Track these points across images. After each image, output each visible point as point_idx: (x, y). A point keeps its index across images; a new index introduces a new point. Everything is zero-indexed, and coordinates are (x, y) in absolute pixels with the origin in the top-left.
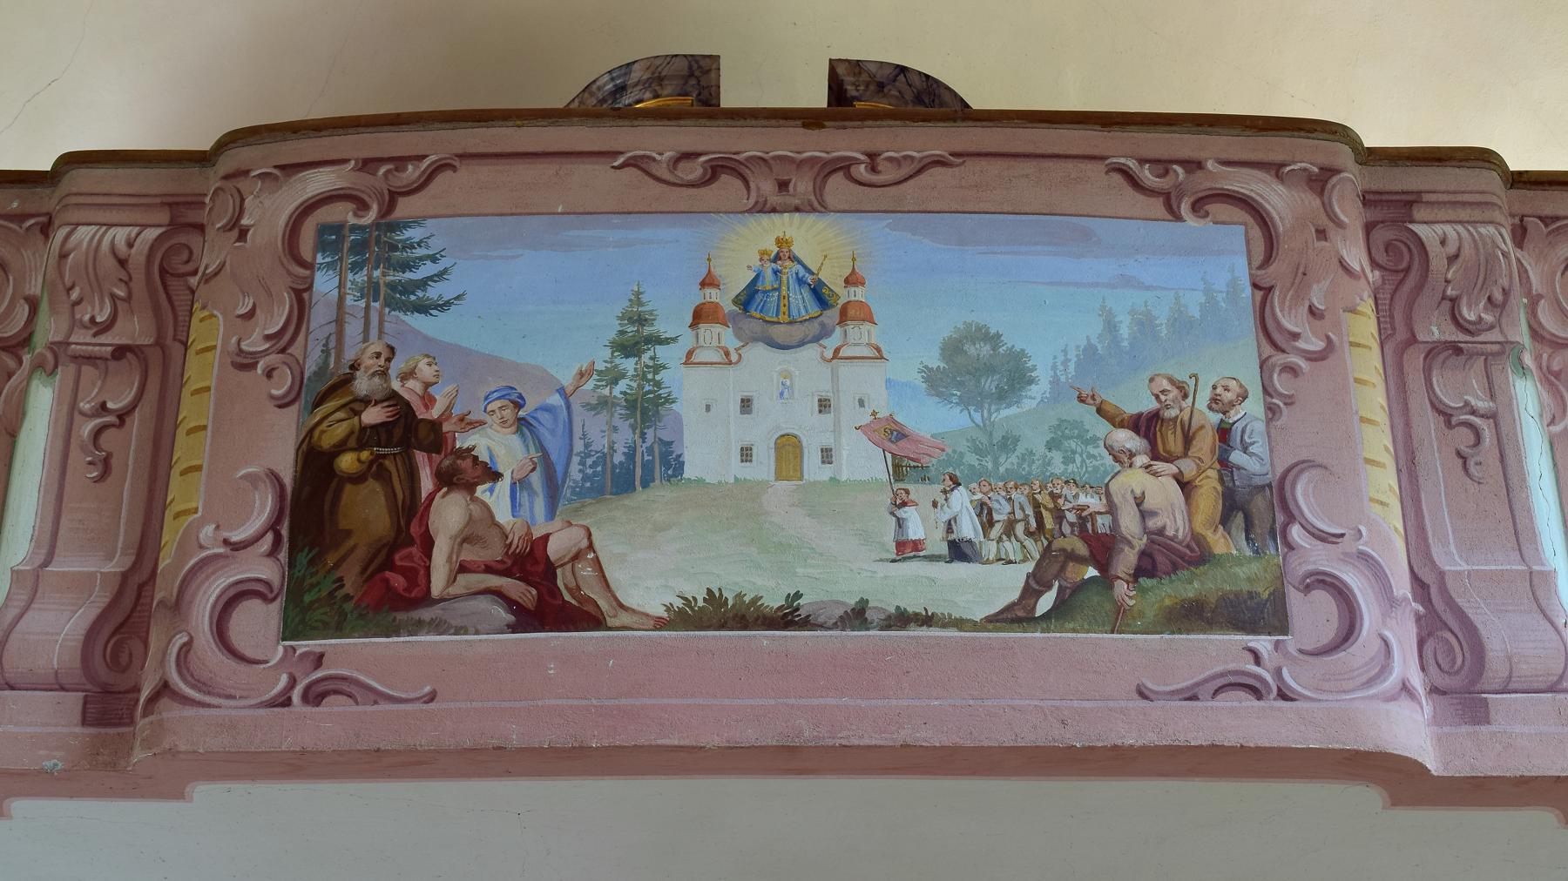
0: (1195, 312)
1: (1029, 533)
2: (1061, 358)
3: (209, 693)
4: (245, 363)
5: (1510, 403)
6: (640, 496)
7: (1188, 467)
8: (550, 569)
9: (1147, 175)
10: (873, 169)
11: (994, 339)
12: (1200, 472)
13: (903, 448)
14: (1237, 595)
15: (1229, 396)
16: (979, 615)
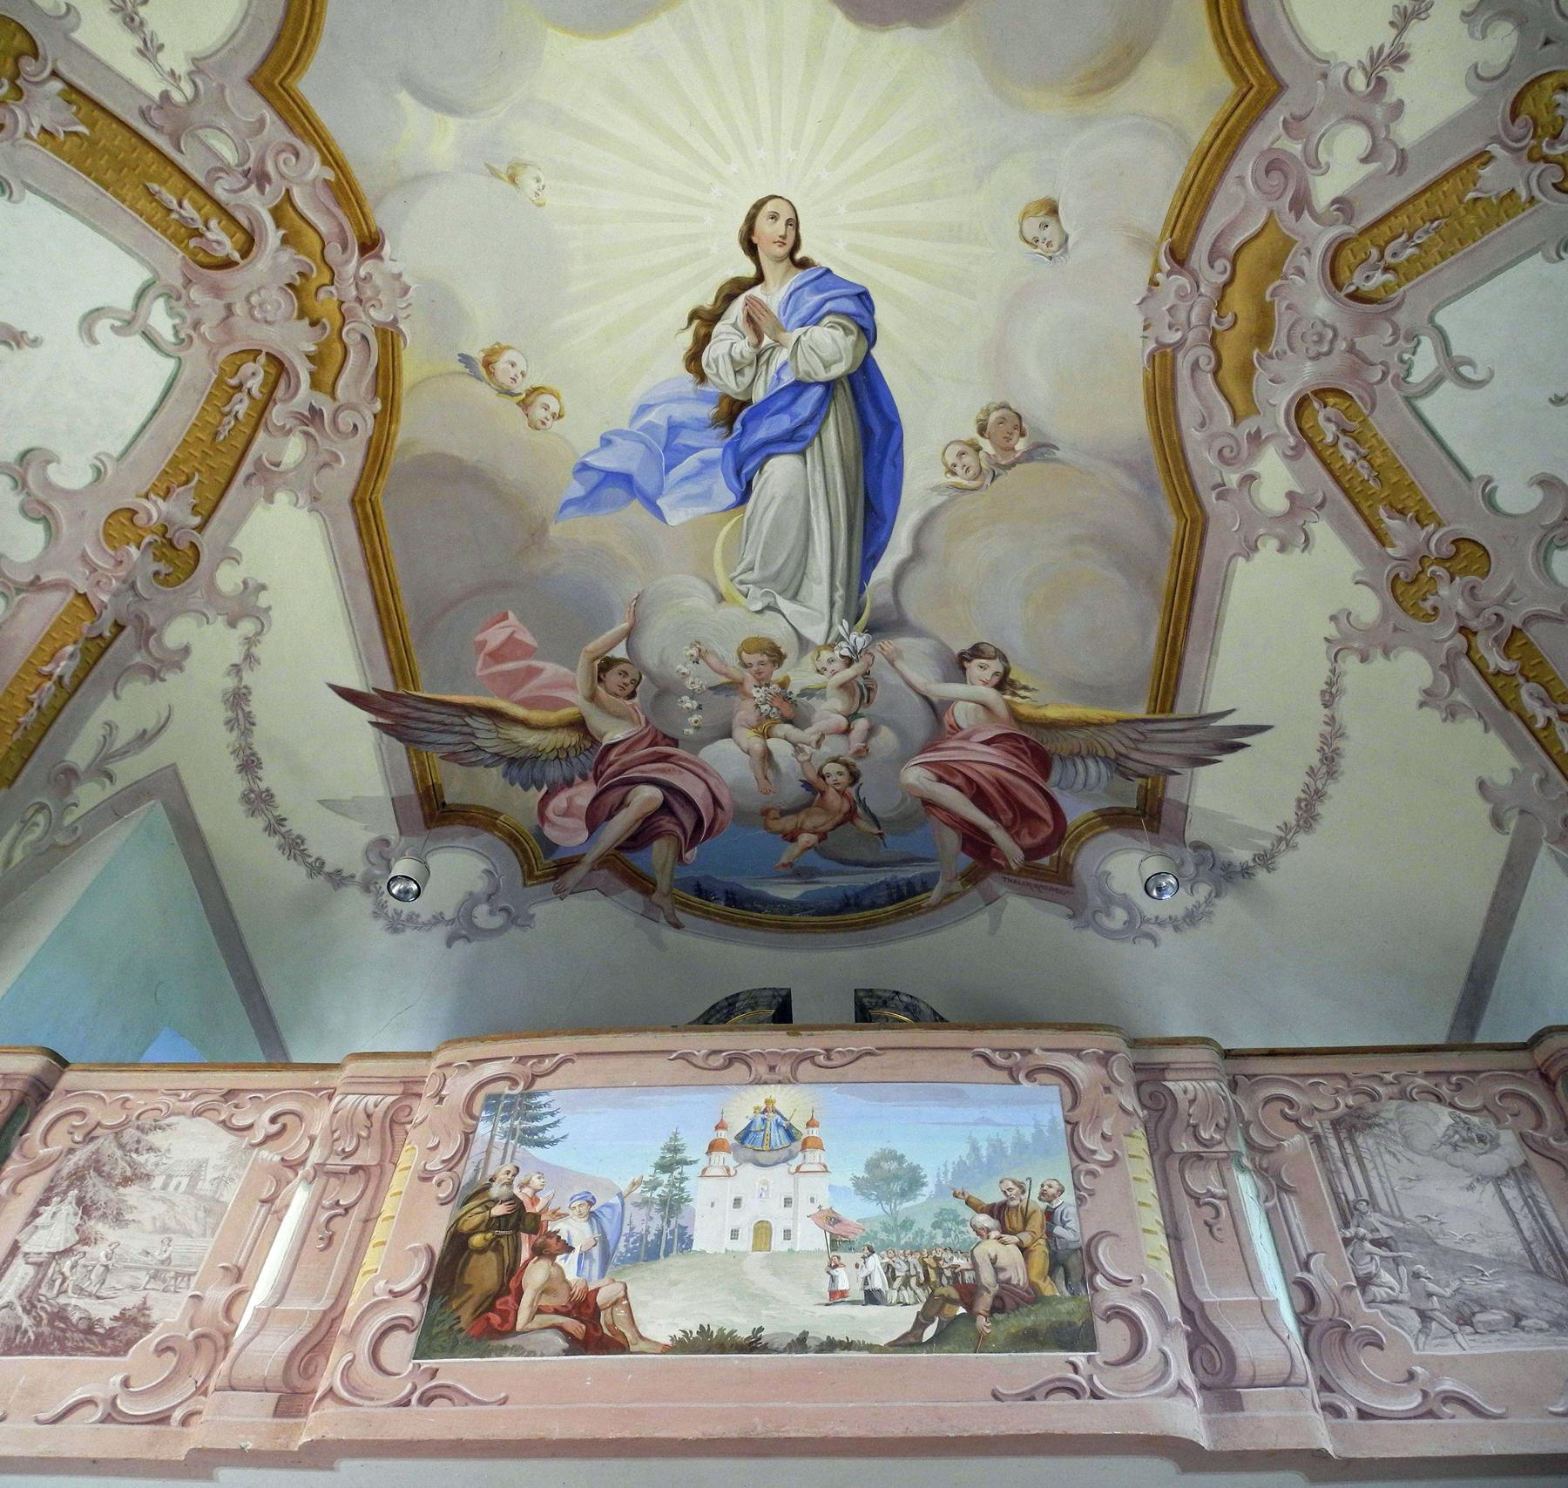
0: (1028, 1138)
1: (919, 1284)
2: (943, 1169)
3: (357, 1396)
4: (426, 1178)
5: (1236, 1189)
6: (663, 1262)
7: (1026, 1238)
8: (597, 1311)
9: (998, 1058)
10: (829, 1058)
11: (900, 1159)
12: (1034, 1241)
13: (837, 1229)
14: (1061, 1323)
15: (1052, 1191)
16: (883, 1341)
